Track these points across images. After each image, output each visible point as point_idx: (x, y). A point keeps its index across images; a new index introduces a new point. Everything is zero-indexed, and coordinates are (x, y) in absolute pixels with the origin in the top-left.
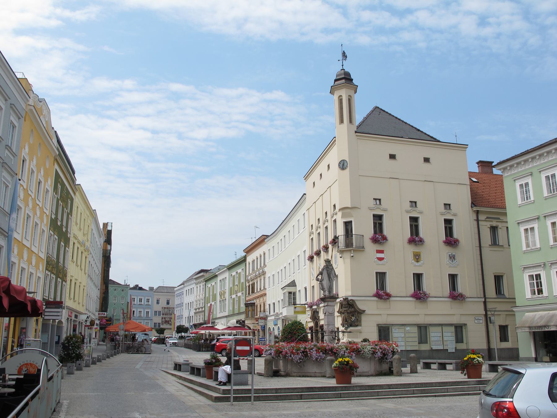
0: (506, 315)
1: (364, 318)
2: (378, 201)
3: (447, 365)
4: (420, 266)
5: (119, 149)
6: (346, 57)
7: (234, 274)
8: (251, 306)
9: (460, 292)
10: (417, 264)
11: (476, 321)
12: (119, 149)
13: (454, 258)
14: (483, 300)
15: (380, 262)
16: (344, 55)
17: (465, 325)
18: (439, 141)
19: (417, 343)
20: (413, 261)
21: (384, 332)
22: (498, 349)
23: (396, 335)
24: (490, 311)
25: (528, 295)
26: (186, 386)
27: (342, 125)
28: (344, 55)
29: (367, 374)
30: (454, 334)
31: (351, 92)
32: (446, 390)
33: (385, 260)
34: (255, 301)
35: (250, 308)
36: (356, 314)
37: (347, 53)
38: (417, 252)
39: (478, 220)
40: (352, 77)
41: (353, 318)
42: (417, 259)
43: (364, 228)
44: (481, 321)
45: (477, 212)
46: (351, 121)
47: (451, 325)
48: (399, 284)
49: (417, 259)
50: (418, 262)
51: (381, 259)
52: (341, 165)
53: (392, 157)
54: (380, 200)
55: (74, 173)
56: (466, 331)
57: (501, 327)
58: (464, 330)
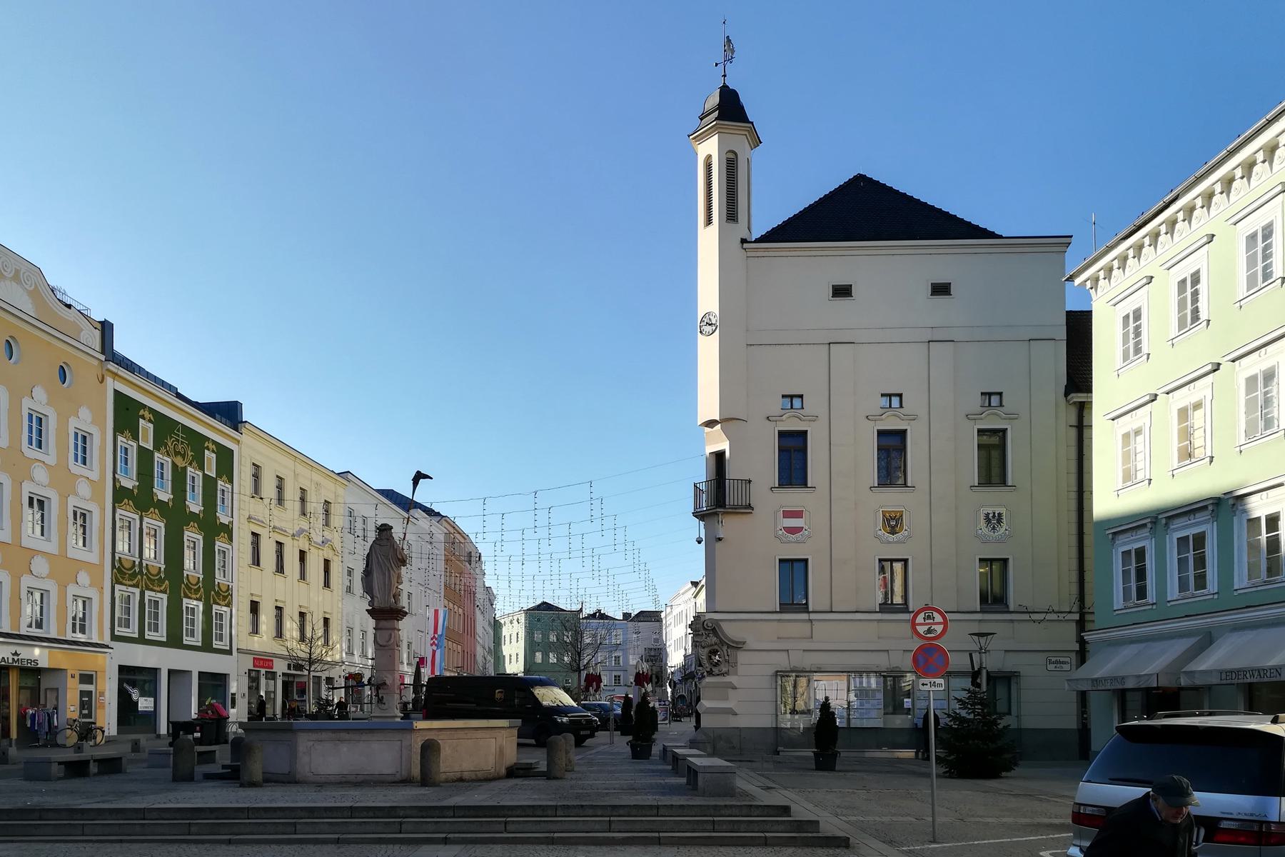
2: (895, 401)
4: (797, 542)
11: (1051, 667)
14: (1077, 617)
15: (792, 537)
18: (1000, 237)
25: (1118, 602)
26: (642, 771)
27: (710, 227)
29: (390, 778)
31: (739, 143)
32: (502, 827)
36: (725, 648)
42: (893, 527)
43: (758, 466)
46: (731, 214)
50: (893, 532)
54: (900, 396)
56: (1019, 690)
58: (1014, 687)
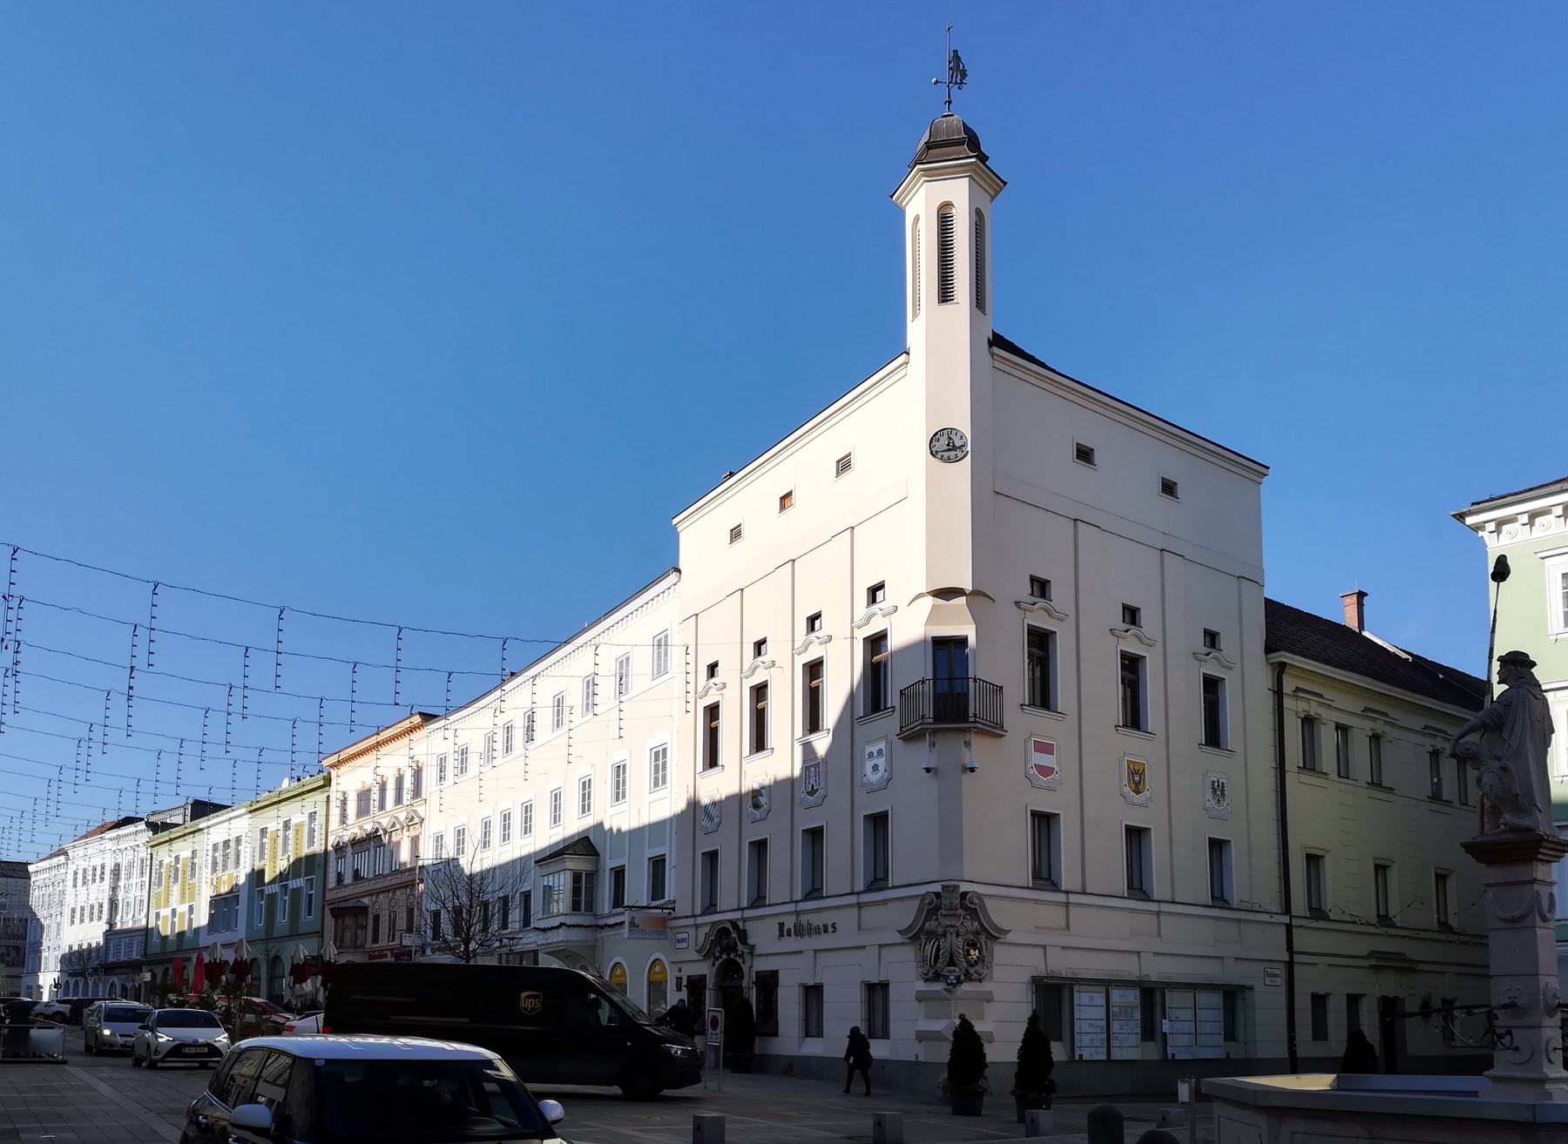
1: (1000, 953)
6: (964, 75)
7: (274, 825)
8: (355, 915)
10: (1136, 798)
13: (1223, 791)
16: (958, 70)
17: (1251, 988)
19: (1220, 1040)
21: (1052, 996)
23: (1088, 1009)
28: (958, 70)
30: (1077, 1015)
34: (366, 901)
35: (349, 921)
39: (1278, 693)
41: (974, 953)
42: (1137, 784)
44: (1279, 981)
45: (1281, 668)
48: (1090, 854)
49: (1137, 784)
51: (1045, 771)
53: (1084, 454)
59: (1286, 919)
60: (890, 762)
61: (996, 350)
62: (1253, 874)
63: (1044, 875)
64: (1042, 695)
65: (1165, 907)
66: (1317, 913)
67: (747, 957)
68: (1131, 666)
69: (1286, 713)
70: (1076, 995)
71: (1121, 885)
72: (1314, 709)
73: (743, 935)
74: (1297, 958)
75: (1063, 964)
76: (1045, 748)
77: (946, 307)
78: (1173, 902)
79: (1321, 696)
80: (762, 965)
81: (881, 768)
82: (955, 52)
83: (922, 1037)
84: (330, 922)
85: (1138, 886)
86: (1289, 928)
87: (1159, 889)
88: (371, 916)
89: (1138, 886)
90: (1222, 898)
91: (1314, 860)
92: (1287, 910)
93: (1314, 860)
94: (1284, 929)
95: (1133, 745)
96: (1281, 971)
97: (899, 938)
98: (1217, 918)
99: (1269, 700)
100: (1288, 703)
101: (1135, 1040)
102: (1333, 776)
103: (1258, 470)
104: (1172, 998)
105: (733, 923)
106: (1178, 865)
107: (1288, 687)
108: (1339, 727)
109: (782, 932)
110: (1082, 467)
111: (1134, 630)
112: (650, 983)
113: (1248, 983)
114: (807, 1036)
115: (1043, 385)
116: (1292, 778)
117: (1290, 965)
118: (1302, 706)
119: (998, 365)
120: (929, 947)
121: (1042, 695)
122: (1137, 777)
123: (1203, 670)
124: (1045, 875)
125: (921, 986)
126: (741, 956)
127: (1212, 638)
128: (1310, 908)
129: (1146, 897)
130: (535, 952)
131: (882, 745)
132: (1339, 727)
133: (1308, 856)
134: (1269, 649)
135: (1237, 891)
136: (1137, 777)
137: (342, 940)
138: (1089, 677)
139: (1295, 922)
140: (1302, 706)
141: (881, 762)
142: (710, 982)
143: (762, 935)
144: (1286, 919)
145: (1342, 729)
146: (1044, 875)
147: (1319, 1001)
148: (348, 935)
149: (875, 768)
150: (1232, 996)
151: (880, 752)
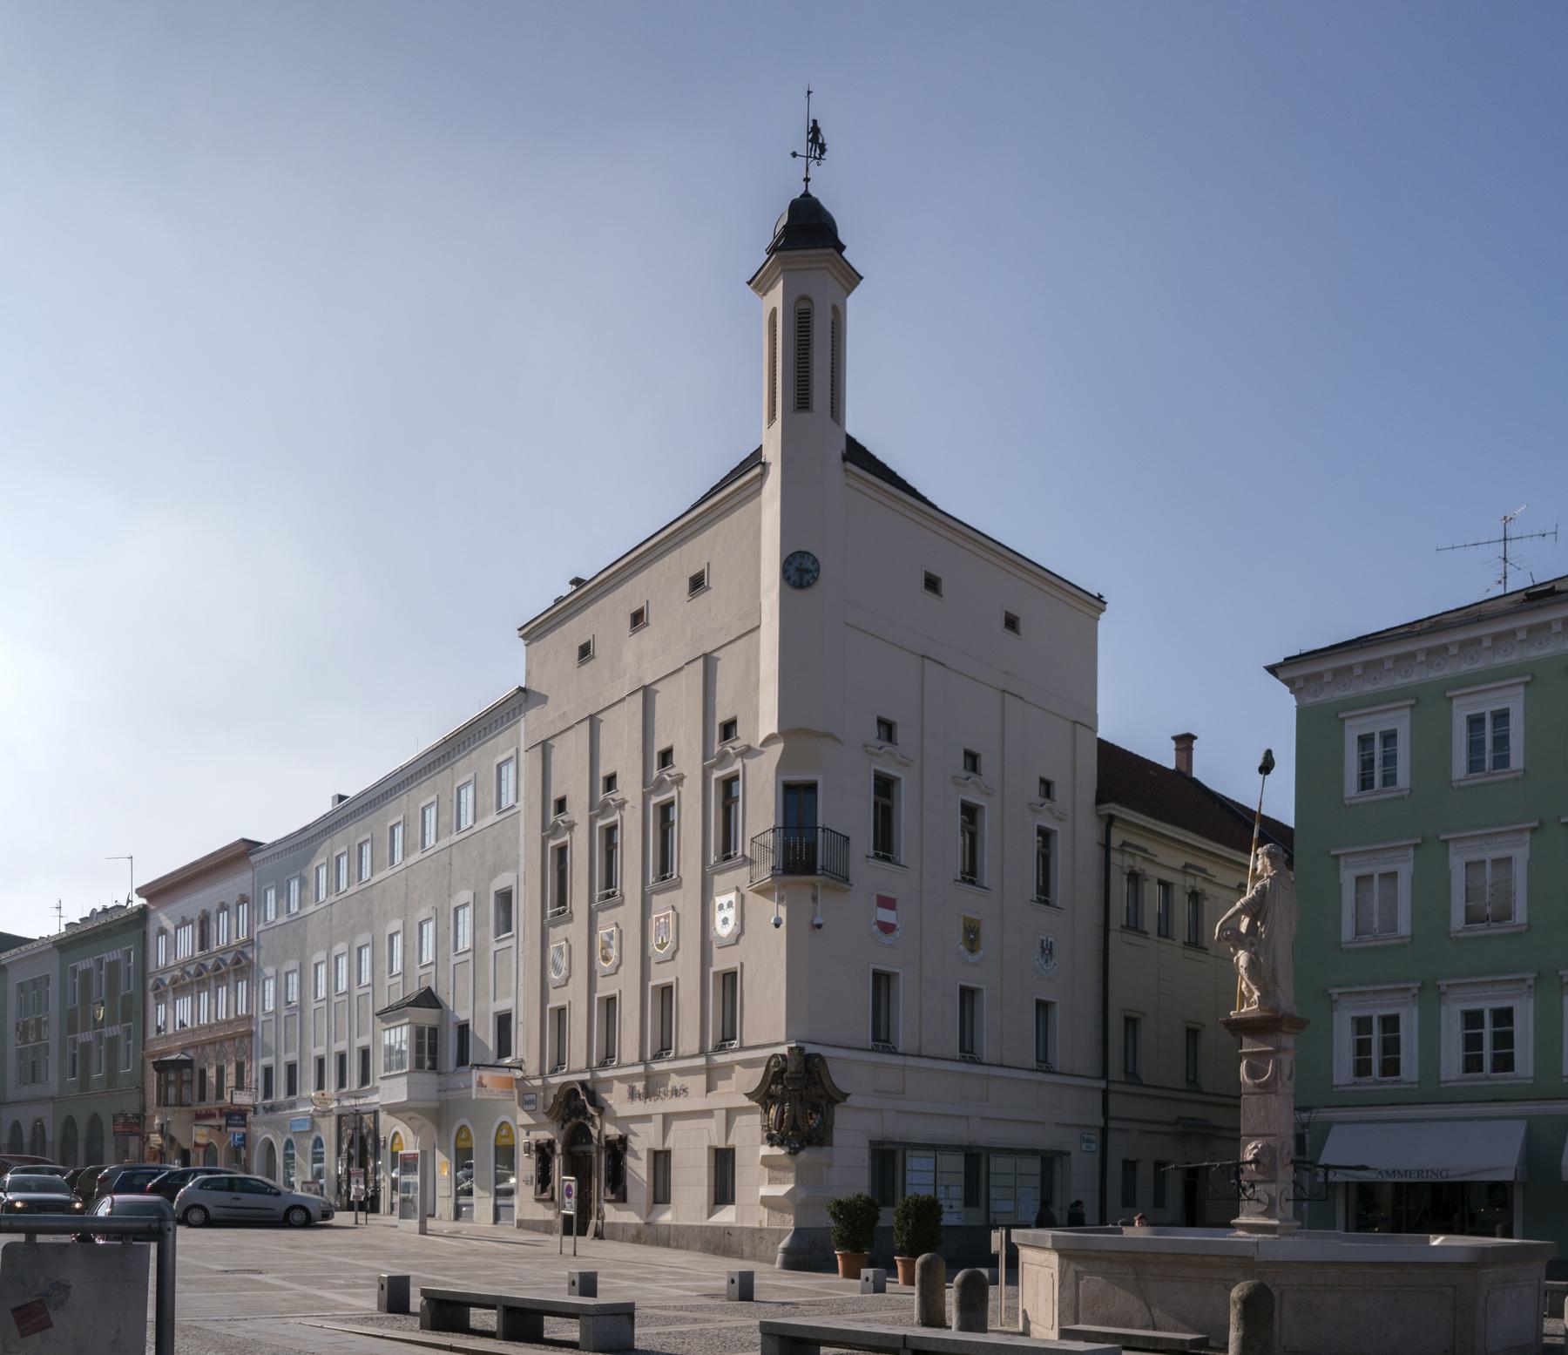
0: (1142, 1132)
3: (473, 1310)
5: (713, 1296)
6: (823, 149)
9: (724, 1283)
10: (971, 958)
12: (713, 1296)
15: (885, 939)
17: (1068, 1154)
20: (962, 948)
22: (836, 1272)
24: (657, 1320)
33: (897, 934)
37: (826, 135)
38: (972, 920)
39: (1106, 846)
40: (842, 237)
45: (1111, 820)
47: (1033, 1152)
48: (924, 1015)
51: (887, 928)
52: (794, 576)
55: (242, 853)
57: (1125, 1162)
59: (1102, 1084)
60: (742, 917)
61: (849, 465)
62: (1074, 1039)
63: (882, 1039)
64: (884, 845)
65: (910, 1061)
66: (1132, 1076)
67: (598, 1121)
68: (884, 786)
69: (1113, 868)
70: (908, 1160)
71: (954, 1048)
72: (1139, 865)
73: (593, 1098)
74: (1111, 1124)
75: (898, 1129)
76: (887, 903)
77: (804, 416)
78: (919, 1056)
79: (1145, 851)
80: (612, 1131)
81: (732, 922)
82: (815, 122)
83: (767, 1202)
84: (152, 1077)
85: (968, 1052)
86: (1105, 1092)
87: (987, 1052)
88: (197, 1071)
89: (968, 1052)
90: (1194, 1081)
91: (1131, 1022)
92: (1105, 1075)
93: (1131, 1022)
94: (1100, 1095)
95: (969, 901)
96: (1095, 1136)
97: (747, 1102)
98: (1039, 1082)
99: (1096, 853)
100: (1115, 858)
101: (958, 1205)
102: (1153, 935)
103: (1098, 603)
104: (998, 1165)
105: (583, 1084)
106: (1008, 1028)
107: (1116, 840)
108: (1160, 882)
109: (632, 1094)
110: (929, 597)
111: (1048, 804)
112: (457, 1150)
113: (1066, 1148)
114: (655, 1202)
115: (1020, 574)
116: (1114, 937)
117: (1104, 1131)
118: (1128, 861)
119: (853, 483)
120: (773, 1112)
121: (884, 845)
122: (972, 935)
123: (874, 767)
124: (883, 1036)
125: (765, 1150)
126: (591, 1118)
127: (972, 760)
128: (1126, 1073)
129: (1050, 1071)
130: (376, 1112)
131: (732, 897)
132: (1160, 882)
133: (1188, 1030)
134: (1100, 800)
135: (1059, 1058)
136: (972, 935)
137: (166, 1097)
138: (928, 827)
139: (1112, 1087)
140: (1128, 861)
141: (731, 914)
142: (558, 1148)
143: (617, 1100)
144: (1102, 1084)
145: (1166, 886)
146: (882, 1039)
147: (1130, 1166)
148: (172, 1091)
149: (725, 921)
150: (1050, 1160)
151: (730, 904)
